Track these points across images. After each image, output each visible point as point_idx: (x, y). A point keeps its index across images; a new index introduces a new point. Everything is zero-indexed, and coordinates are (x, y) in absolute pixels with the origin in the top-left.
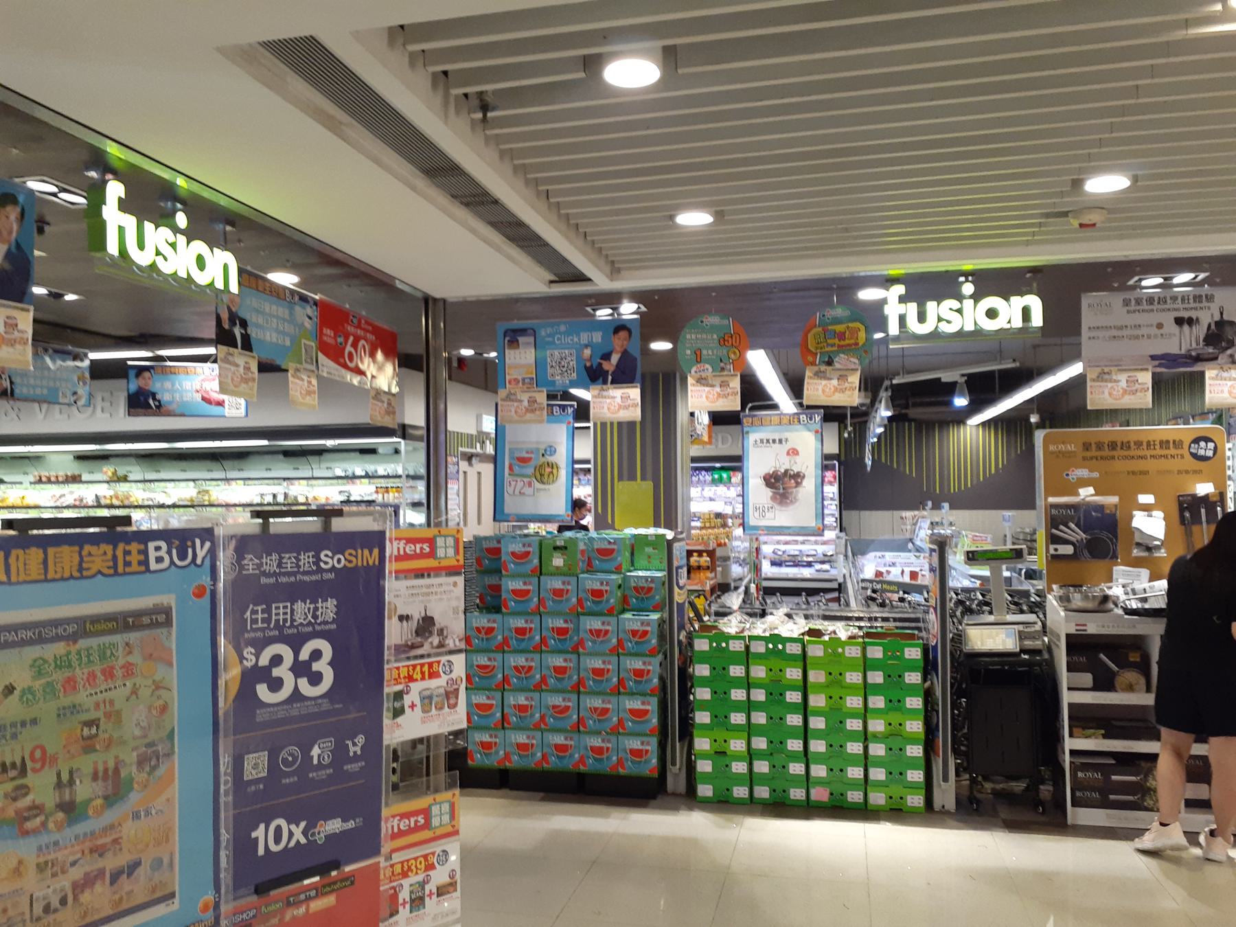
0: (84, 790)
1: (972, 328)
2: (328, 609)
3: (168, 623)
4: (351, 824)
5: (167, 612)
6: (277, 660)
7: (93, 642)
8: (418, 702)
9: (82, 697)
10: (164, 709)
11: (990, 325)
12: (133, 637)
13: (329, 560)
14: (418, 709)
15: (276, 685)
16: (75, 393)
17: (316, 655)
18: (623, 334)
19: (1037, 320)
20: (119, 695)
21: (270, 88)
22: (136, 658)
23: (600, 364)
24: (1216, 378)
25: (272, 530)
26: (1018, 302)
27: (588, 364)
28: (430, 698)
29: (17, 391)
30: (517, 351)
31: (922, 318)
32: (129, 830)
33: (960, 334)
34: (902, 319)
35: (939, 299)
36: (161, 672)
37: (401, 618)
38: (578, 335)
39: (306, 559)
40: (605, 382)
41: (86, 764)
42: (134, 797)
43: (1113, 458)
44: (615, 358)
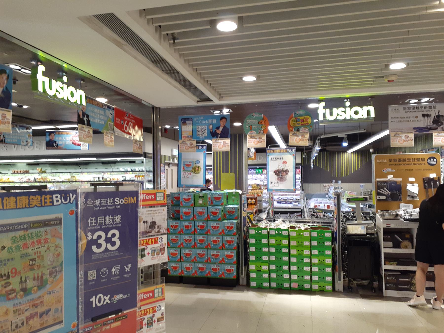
0: (30, 284)
1: (349, 118)
2: (118, 219)
3: (60, 224)
4: (126, 296)
5: (60, 220)
6: (99, 237)
7: (34, 231)
8: (150, 252)
9: (29, 250)
10: (59, 255)
11: (356, 117)
12: (48, 229)
13: (118, 201)
14: (150, 255)
15: (99, 246)
16: (27, 141)
17: (114, 235)
18: (224, 120)
19: (373, 115)
20: (43, 249)
21: (97, 31)
22: (49, 236)
23: (216, 131)
24: (437, 136)
25: (98, 190)
26: (366, 108)
27: (211, 131)
28: (155, 251)
29: (6, 141)
30: (186, 126)
31: (331, 114)
32: (46, 298)
33: (345, 120)
34: (324, 115)
35: (337, 107)
36: (58, 241)
37: (144, 222)
38: (208, 120)
39: (110, 201)
40: (217, 137)
41: (31, 274)
42: (48, 286)
43: (400, 164)
44: (221, 129)
